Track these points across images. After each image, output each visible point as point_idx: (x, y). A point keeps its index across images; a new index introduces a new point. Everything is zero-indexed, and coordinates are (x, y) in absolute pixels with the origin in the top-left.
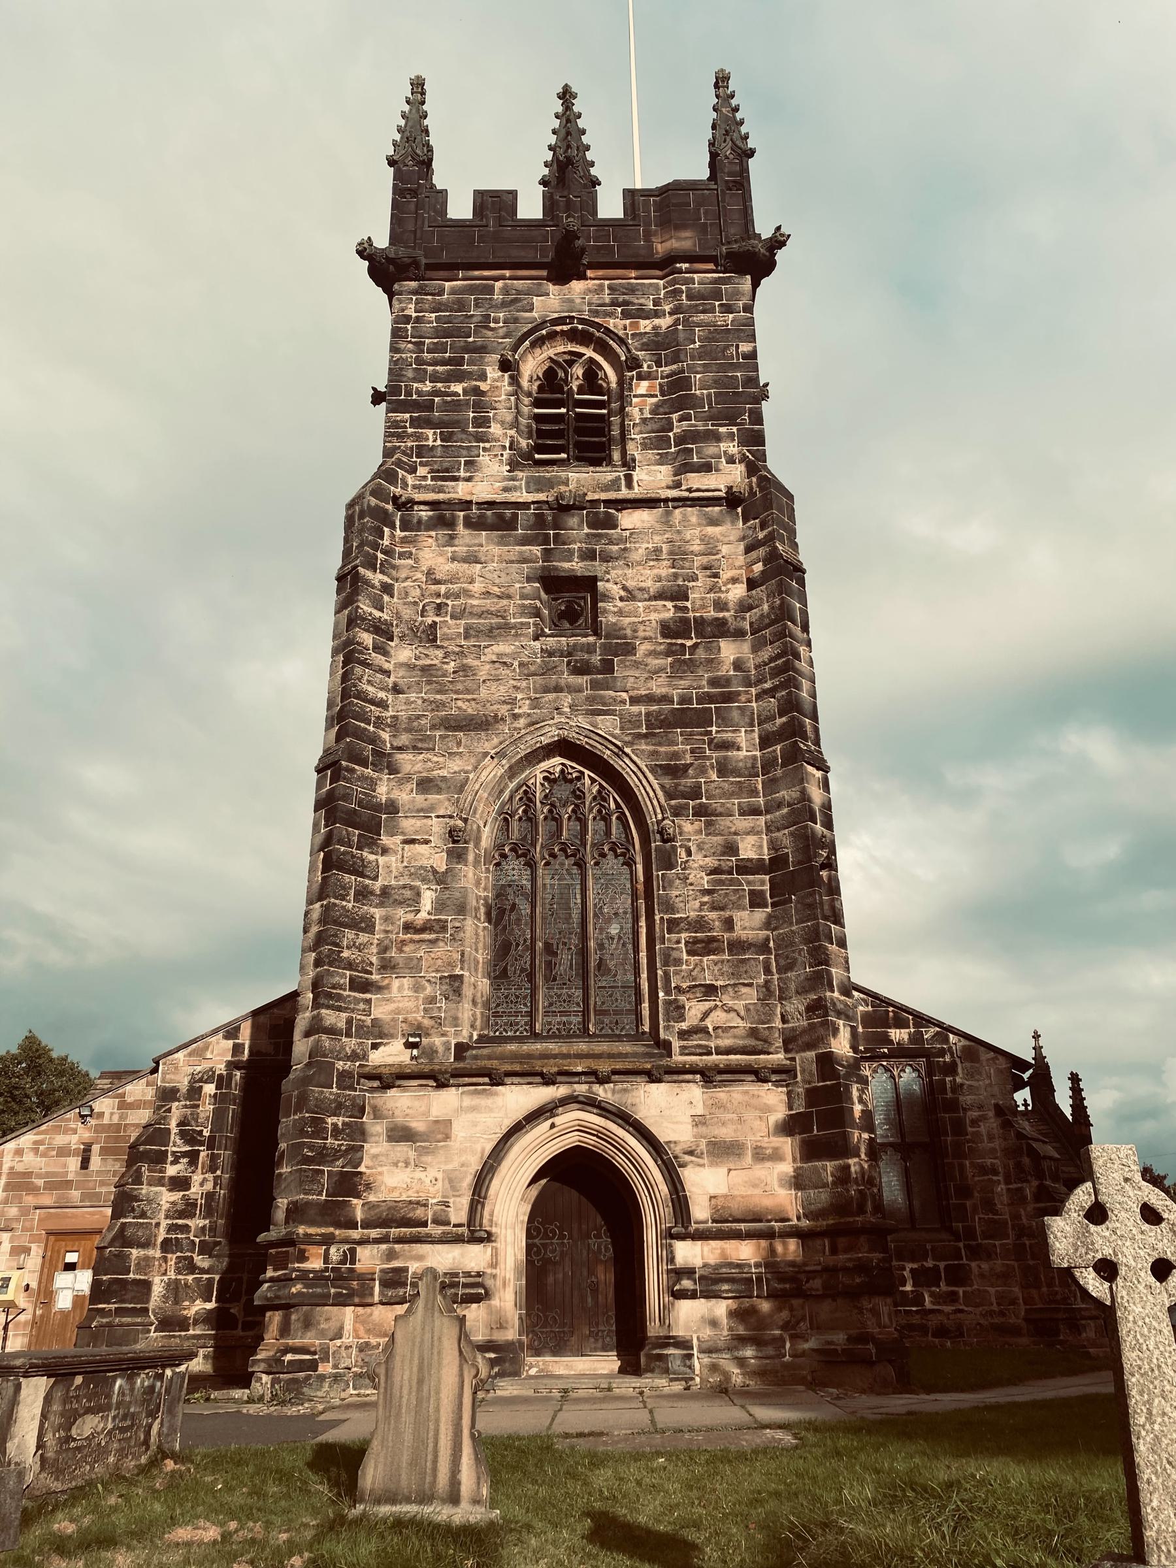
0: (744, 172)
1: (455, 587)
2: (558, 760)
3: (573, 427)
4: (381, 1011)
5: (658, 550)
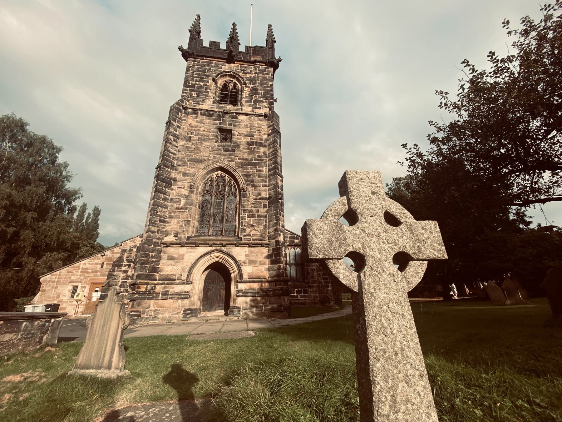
0: (273, 45)
1: (196, 129)
2: (220, 172)
3: (229, 96)
4: (168, 228)
5: (247, 125)
